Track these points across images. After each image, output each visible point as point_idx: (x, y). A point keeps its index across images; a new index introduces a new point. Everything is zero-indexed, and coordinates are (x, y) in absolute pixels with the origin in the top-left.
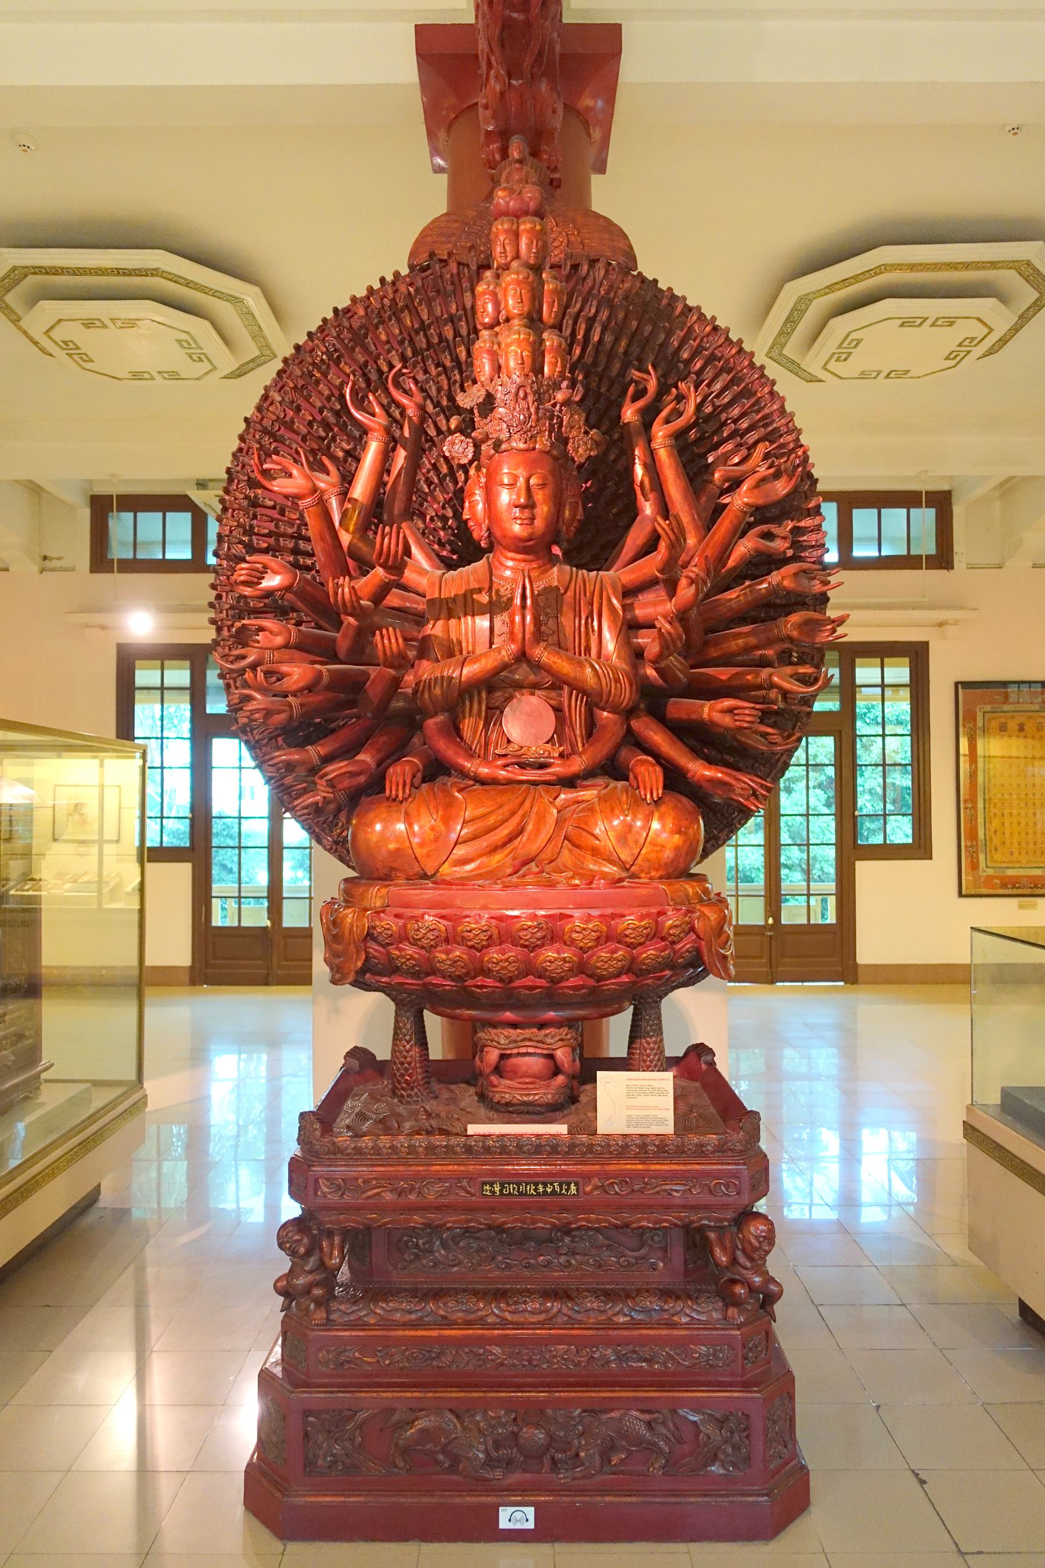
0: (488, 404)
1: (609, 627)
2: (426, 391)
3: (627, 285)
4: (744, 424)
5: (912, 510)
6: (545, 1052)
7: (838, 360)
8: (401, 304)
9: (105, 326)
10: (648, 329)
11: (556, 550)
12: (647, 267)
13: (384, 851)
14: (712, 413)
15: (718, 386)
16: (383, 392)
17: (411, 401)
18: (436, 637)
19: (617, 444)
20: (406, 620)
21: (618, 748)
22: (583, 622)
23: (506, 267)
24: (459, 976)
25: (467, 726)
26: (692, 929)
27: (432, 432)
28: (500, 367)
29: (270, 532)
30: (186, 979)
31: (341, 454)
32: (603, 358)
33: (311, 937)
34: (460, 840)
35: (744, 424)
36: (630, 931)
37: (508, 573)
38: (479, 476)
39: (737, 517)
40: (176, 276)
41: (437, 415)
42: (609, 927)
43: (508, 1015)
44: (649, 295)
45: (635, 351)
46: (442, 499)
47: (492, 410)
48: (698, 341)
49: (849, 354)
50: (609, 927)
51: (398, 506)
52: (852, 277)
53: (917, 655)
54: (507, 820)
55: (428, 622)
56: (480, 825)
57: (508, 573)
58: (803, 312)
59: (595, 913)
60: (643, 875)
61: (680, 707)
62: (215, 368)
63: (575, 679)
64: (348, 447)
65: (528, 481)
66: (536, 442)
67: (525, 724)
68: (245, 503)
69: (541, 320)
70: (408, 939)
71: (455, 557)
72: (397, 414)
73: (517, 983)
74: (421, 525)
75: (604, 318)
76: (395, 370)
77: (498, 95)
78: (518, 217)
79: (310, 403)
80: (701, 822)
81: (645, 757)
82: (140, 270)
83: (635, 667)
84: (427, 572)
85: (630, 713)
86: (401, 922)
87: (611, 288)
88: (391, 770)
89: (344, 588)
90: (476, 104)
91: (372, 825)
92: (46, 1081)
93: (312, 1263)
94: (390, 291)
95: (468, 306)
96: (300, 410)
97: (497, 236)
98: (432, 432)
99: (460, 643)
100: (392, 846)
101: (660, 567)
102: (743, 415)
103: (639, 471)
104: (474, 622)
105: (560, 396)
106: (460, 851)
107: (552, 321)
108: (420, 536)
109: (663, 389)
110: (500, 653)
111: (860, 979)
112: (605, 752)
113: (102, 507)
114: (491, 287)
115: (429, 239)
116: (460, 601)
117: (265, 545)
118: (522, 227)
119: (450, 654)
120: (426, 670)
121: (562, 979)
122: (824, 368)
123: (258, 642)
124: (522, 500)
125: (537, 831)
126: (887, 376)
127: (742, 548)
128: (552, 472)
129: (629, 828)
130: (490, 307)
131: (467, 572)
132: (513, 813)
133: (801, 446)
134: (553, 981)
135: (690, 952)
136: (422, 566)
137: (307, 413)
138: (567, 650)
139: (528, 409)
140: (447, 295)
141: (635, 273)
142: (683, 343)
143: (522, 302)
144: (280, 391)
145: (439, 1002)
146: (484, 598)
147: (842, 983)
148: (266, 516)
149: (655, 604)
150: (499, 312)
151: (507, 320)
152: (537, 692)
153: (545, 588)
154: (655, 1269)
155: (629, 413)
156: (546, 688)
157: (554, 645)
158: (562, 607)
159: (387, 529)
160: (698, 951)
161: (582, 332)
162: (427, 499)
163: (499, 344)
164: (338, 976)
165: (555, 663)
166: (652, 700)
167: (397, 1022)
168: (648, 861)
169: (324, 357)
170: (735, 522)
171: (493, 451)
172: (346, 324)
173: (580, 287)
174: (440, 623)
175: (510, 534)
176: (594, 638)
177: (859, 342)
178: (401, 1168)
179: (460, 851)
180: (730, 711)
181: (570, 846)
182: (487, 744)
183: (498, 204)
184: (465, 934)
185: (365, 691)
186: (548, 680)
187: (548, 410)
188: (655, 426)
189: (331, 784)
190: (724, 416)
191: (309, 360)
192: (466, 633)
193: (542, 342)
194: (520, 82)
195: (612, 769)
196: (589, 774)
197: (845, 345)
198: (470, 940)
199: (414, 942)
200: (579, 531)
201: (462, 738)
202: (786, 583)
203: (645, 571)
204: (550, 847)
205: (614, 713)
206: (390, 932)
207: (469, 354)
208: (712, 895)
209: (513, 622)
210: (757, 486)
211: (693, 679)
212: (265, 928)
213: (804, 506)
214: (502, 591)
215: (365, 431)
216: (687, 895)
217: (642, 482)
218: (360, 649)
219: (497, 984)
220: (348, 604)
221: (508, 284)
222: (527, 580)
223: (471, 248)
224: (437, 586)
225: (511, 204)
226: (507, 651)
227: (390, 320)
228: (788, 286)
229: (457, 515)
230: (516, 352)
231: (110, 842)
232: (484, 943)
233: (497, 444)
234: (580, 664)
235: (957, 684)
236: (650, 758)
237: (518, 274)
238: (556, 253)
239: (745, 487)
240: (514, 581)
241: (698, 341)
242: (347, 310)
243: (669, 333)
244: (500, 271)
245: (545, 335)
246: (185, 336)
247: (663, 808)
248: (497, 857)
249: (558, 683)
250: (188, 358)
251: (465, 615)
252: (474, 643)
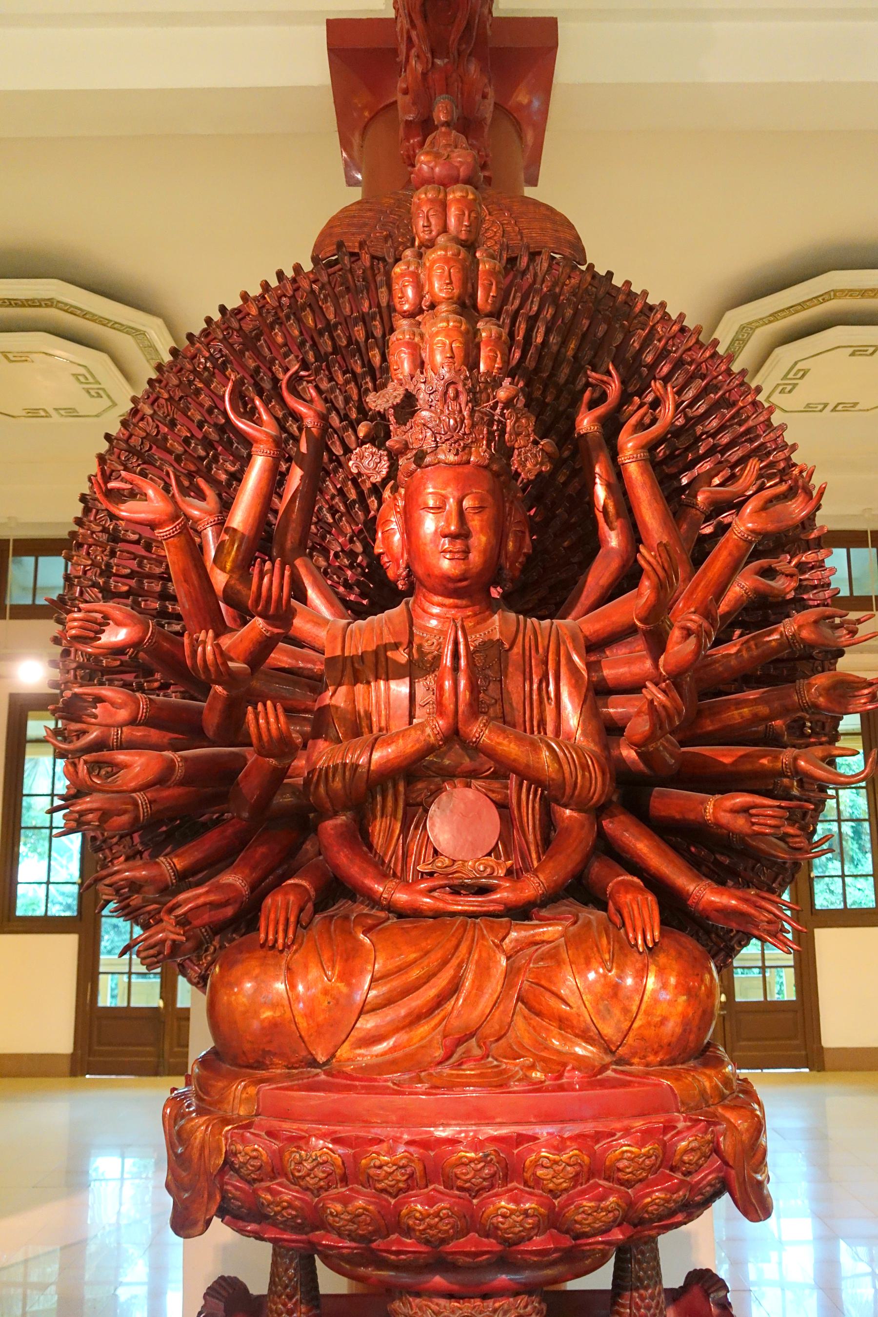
0: (407, 406)
1: (570, 694)
2: (332, 402)
3: (574, 281)
4: (725, 439)
5: (852, 550)
8: (300, 301)
10: (602, 329)
11: (495, 593)
12: (601, 256)
13: (255, 1025)
14: (682, 426)
15: (690, 394)
16: (277, 403)
17: (310, 408)
18: (337, 708)
19: (572, 461)
20: (295, 684)
21: (586, 862)
22: (535, 686)
23: (430, 244)
25: (378, 829)
26: (716, 1150)
27: (338, 451)
28: (423, 363)
29: (132, 571)
30: (66, 1066)
31: (223, 477)
32: (548, 363)
34: (366, 1008)
35: (725, 439)
36: (626, 1163)
37: (434, 623)
38: (395, 499)
39: (737, 546)
40: (72, 306)
41: (345, 429)
42: (592, 1154)
43: (438, 1280)
44: (602, 291)
45: (588, 354)
46: (349, 530)
47: (413, 413)
48: (663, 342)
49: (795, 385)
50: (592, 1154)
51: (291, 540)
52: (799, 304)
54: (434, 975)
55: (326, 689)
56: (396, 983)
57: (434, 623)
58: (745, 342)
59: (570, 1130)
60: (636, 1060)
61: (671, 801)
62: (114, 404)
63: (528, 766)
64: (233, 469)
65: (460, 502)
66: (470, 454)
67: (456, 827)
68: (104, 537)
69: (475, 306)
70: (286, 1175)
71: (365, 602)
72: (294, 429)
73: (450, 1247)
74: (323, 563)
75: (549, 316)
76: (290, 373)
77: (420, 77)
78: (445, 186)
79: (188, 417)
81: (629, 878)
82: (33, 300)
83: (606, 747)
84: (327, 621)
85: (600, 811)
86: (276, 1145)
87: (555, 284)
88: (269, 901)
89: (206, 647)
90: (395, 102)
91: (239, 983)
94: (289, 287)
95: (384, 302)
96: (176, 425)
97: (419, 207)
98: (338, 451)
99: (369, 716)
100: (267, 1014)
101: (643, 614)
102: (721, 429)
103: (600, 492)
104: (388, 689)
105: (502, 394)
106: (368, 1023)
107: (489, 307)
108: (320, 577)
109: (625, 398)
110: (423, 731)
111: (827, 1066)
112: (570, 867)
114: (412, 268)
115: (338, 230)
116: (370, 660)
117: (126, 588)
118: (451, 197)
119: (356, 731)
120: (324, 754)
121: (520, 1240)
123: (96, 717)
124: (453, 528)
125: (479, 988)
127: (737, 589)
128: (492, 492)
129: (614, 990)
130: (410, 292)
131: (380, 621)
132: (445, 962)
133: (794, 465)
134: (505, 1241)
135: (711, 1185)
136: (319, 614)
137: (184, 429)
138: (514, 726)
139: (461, 411)
140: (358, 291)
141: (584, 268)
142: (646, 342)
143: (451, 283)
144: (153, 404)
146: (402, 657)
147: (807, 1070)
148: (128, 552)
149: (629, 662)
150: (422, 297)
151: (432, 306)
152: (475, 783)
153: (484, 643)
155: (585, 421)
156: (487, 777)
157: (496, 718)
158: (506, 667)
159: (268, 565)
161: (522, 333)
162: (328, 529)
163: (422, 336)
165: (499, 744)
166: (631, 792)
167: (274, 1264)
168: (643, 1038)
169: (208, 365)
170: (736, 554)
171: (414, 466)
172: (235, 325)
173: (518, 280)
174: (343, 689)
175: (436, 572)
176: (550, 709)
177: (805, 373)
179: (368, 1023)
180: (745, 810)
181: (526, 1011)
182: (406, 855)
183: (420, 169)
184: (372, 1171)
185: (238, 784)
186: (490, 766)
187: (485, 414)
188: (623, 436)
189: (183, 922)
190: (699, 429)
191: (189, 366)
192: (378, 702)
193: (476, 332)
194: (446, 60)
195: (581, 890)
196: (551, 898)
197: (791, 376)
198: (379, 1181)
199: (296, 1181)
200: (525, 569)
201: (370, 847)
202: (805, 634)
203: (614, 619)
204: (497, 1013)
205: (579, 810)
206: (257, 1163)
207: (384, 359)
209: (441, 688)
210: (764, 508)
211: (686, 761)
212: (157, 1009)
213: (802, 536)
214: (426, 647)
215: (248, 442)
216: (703, 1092)
217: (605, 507)
218: (233, 729)
219: (423, 1248)
220: (212, 669)
221: (434, 262)
222: (460, 633)
223: (389, 236)
224: (340, 640)
225: (437, 170)
226: (431, 727)
227: (288, 318)
228: (729, 314)
229: (368, 549)
230: (444, 344)
232: (401, 1185)
233: (420, 458)
234: (535, 747)
236: (635, 879)
237: (446, 251)
238: (489, 244)
239: (748, 509)
240: (443, 633)
241: (663, 342)
242: (237, 311)
243: (628, 334)
244: (423, 250)
245: (480, 325)
246: (82, 371)
247: (662, 959)
248: (423, 1029)
249: (503, 770)
250: (87, 395)
251: (377, 678)
252: (388, 717)
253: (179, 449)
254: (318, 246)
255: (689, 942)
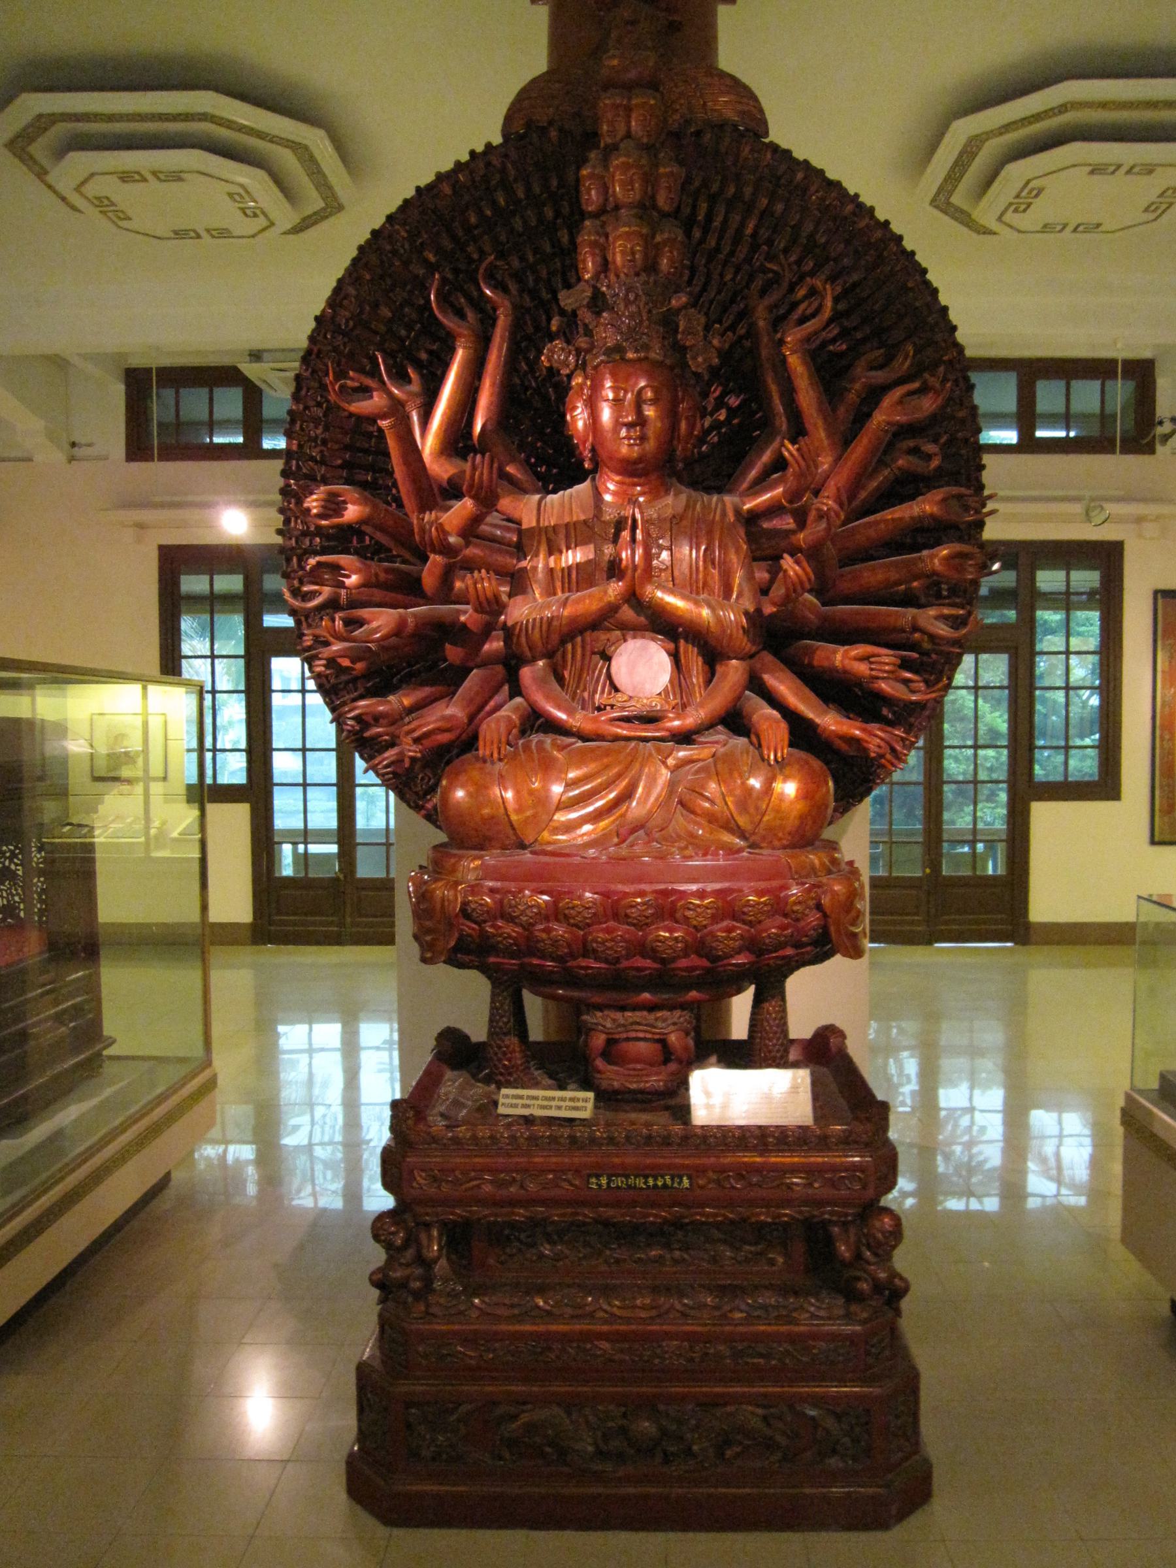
6: (657, 1037)
7: (1016, 211)
9: (145, 180)
24: (562, 957)
33: (392, 889)
34: (562, 806)
49: (1029, 205)
53: (1107, 557)
58: (974, 155)
62: (272, 224)
80: (831, 784)
92: (110, 1058)
93: (410, 1254)
100: (486, 811)
113: (138, 383)
122: (1000, 219)
125: (647, 793)
126: (1075, 230)
132: (619, 776)
134: (663, 961)
145: (540, 981)
151: (617, 208)
154: (773, 1265)
160: (825, 928)
164: (429, 955)
177: (1040, 191)
178: (501, 1160)
195: (734, 721)
196: (709, 726)
197: (1024, 194)
208: (843, 866)
210: (900, 402)
231: (156, 779)
235: (1156, 593)
251: (568, 548)
253: (382, 328)
254: (509, 119)
255: (816, 764)
